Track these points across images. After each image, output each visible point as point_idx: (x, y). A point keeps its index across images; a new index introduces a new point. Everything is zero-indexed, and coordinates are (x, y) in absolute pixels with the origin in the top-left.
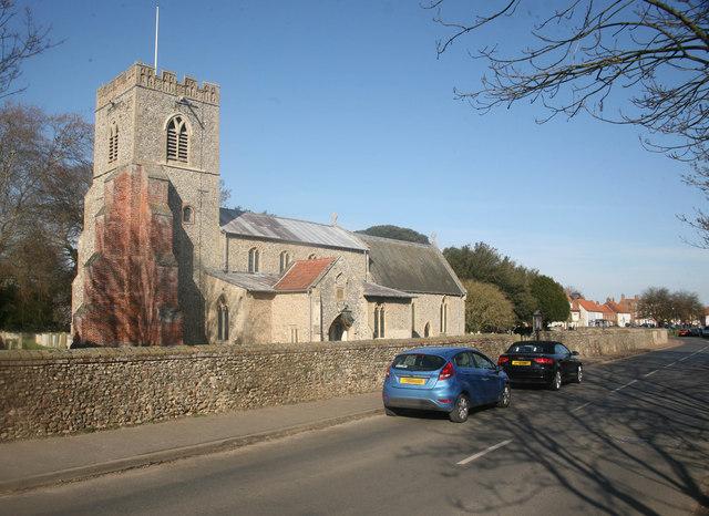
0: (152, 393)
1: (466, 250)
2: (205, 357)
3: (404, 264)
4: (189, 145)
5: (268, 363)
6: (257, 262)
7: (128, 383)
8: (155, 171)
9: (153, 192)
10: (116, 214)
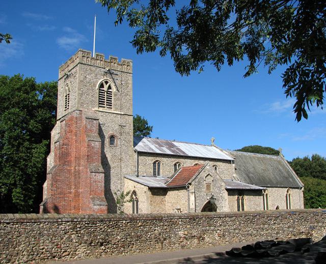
0: (28, 244)
1: (306, 159)
2: (68, 222)
3: (260, 167)
4: (113, 98)
5: (116, 226)
6: (159, 168)
7: (10, 237)
8: (90, 114)
9: (89, 127)
10: (66, 141)
